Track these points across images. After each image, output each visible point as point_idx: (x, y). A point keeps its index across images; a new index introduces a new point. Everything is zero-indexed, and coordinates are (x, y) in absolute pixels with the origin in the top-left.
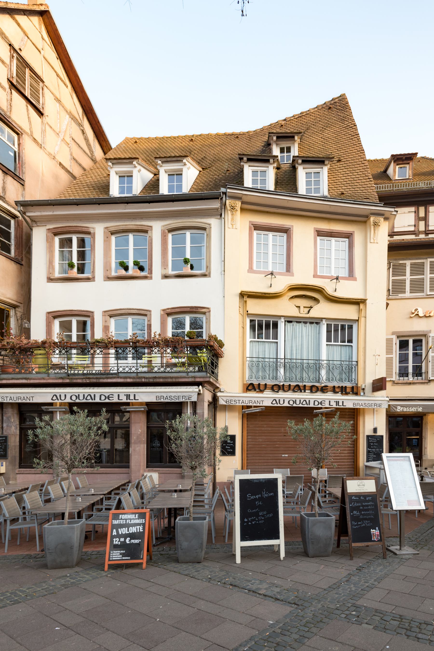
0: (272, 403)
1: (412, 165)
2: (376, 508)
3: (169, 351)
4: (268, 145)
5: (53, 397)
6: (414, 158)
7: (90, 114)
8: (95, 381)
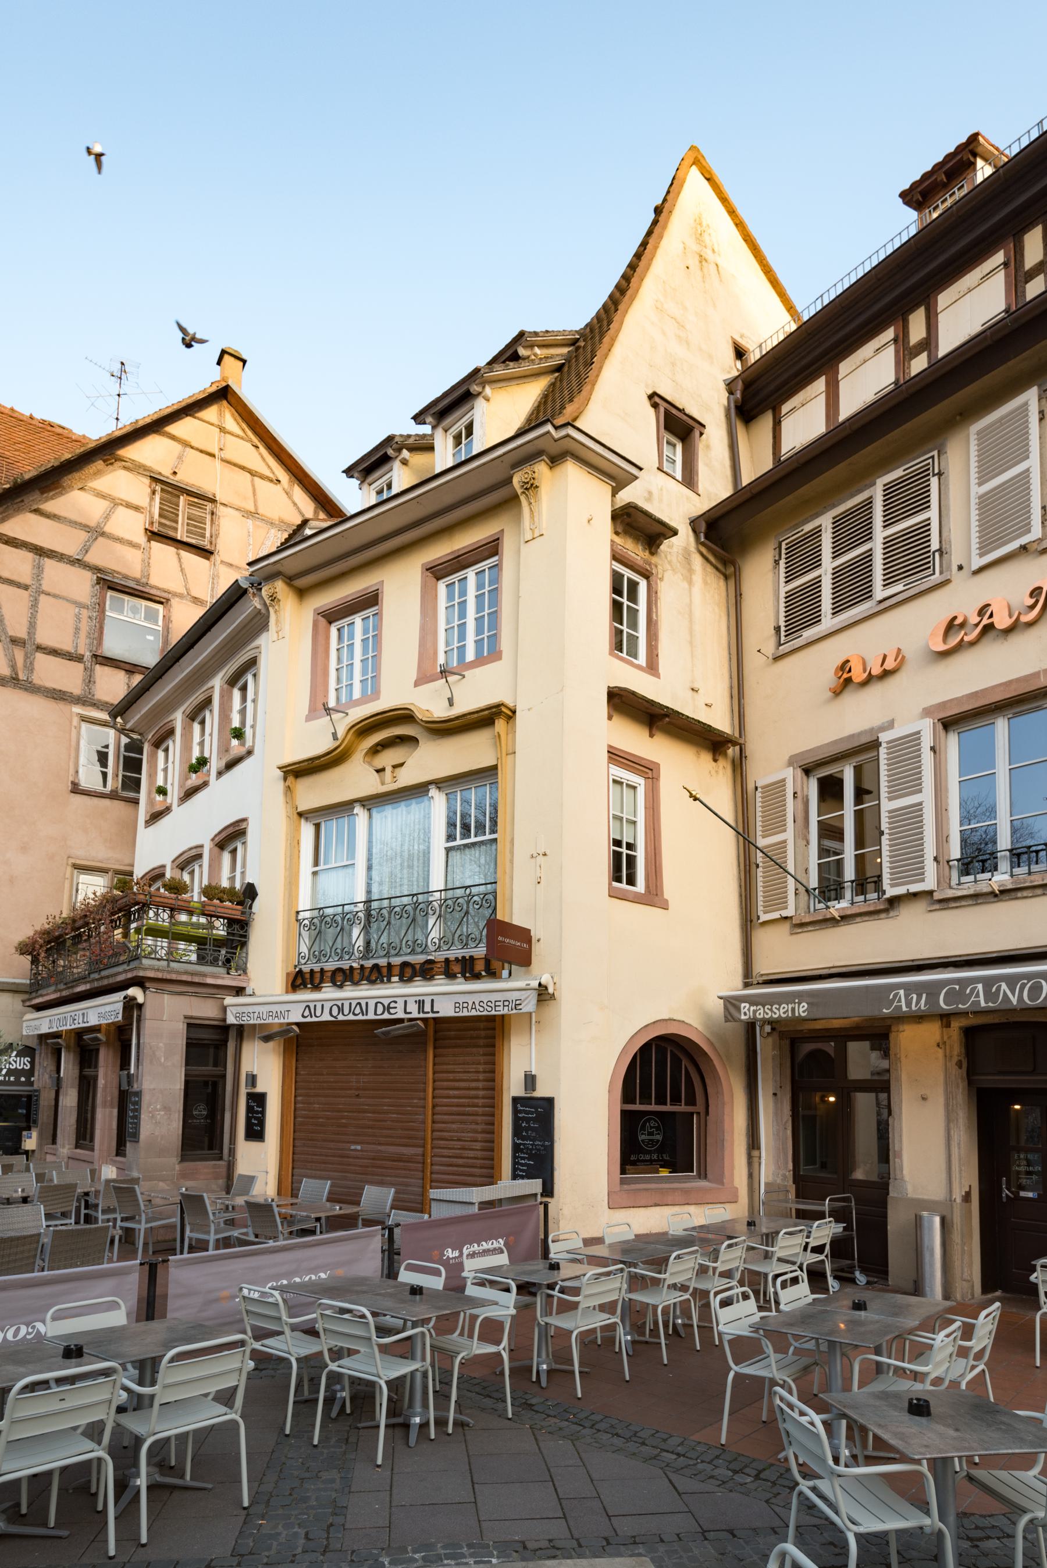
0: (303, 1016)
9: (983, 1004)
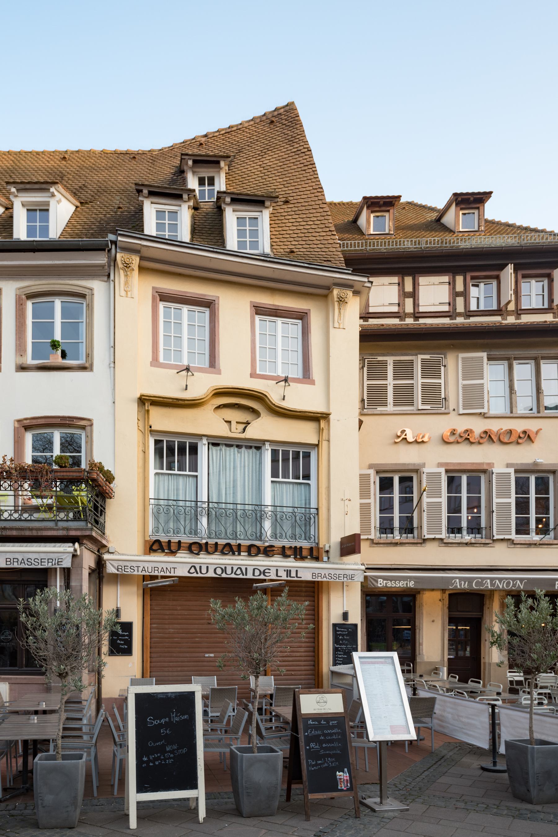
1: (394, 213)
2: (344, 740)
3: (26, 486)
4: (181, 172)
6: (396, 203)
9: (490, 587)
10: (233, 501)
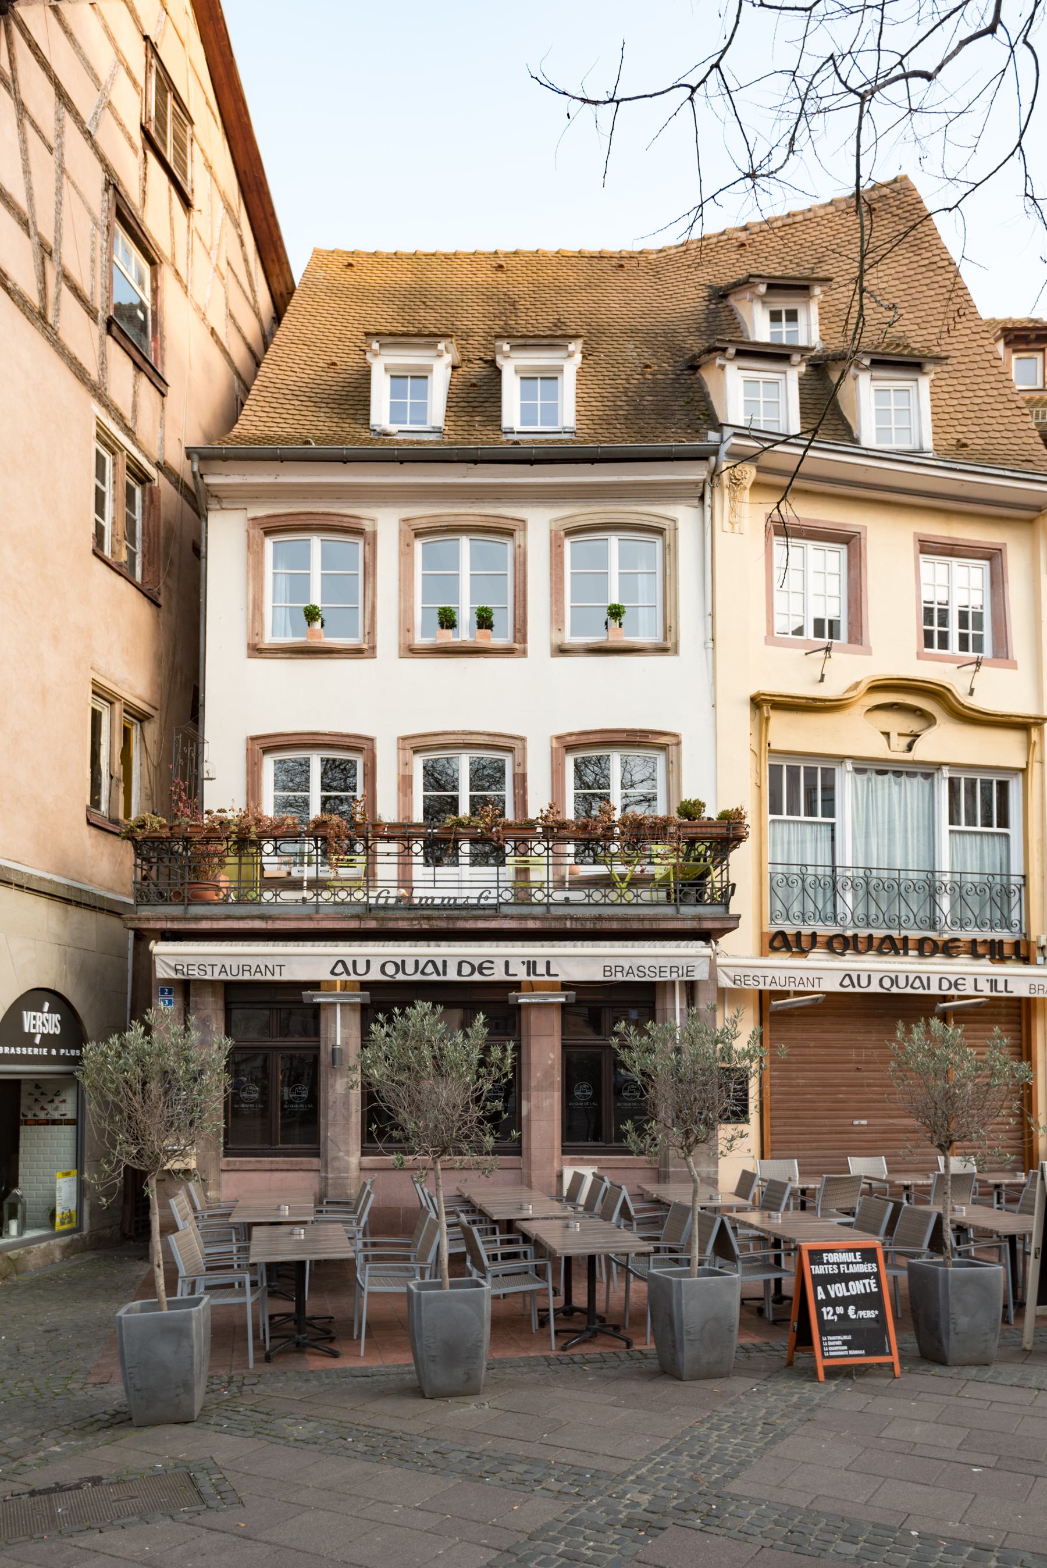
0: (841, 985)
5: (334, 967)
7: (255, 193)
8: (443, 925)
10: (889, 864)
